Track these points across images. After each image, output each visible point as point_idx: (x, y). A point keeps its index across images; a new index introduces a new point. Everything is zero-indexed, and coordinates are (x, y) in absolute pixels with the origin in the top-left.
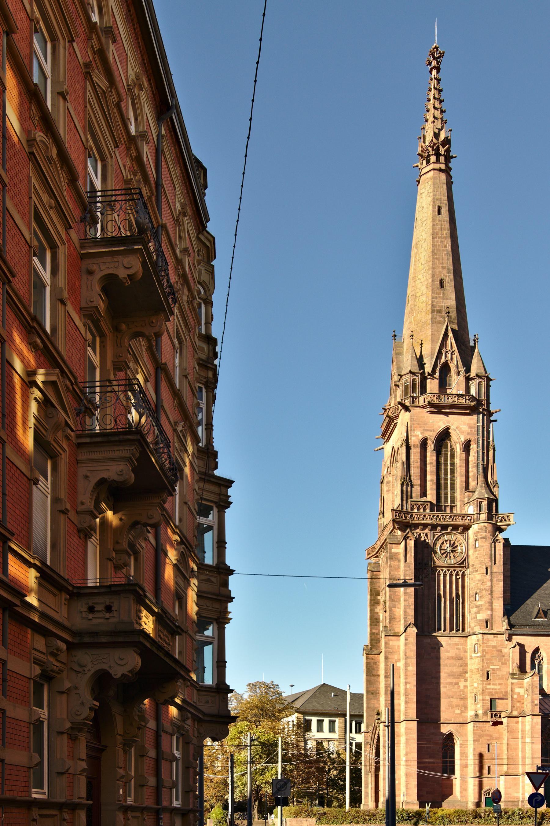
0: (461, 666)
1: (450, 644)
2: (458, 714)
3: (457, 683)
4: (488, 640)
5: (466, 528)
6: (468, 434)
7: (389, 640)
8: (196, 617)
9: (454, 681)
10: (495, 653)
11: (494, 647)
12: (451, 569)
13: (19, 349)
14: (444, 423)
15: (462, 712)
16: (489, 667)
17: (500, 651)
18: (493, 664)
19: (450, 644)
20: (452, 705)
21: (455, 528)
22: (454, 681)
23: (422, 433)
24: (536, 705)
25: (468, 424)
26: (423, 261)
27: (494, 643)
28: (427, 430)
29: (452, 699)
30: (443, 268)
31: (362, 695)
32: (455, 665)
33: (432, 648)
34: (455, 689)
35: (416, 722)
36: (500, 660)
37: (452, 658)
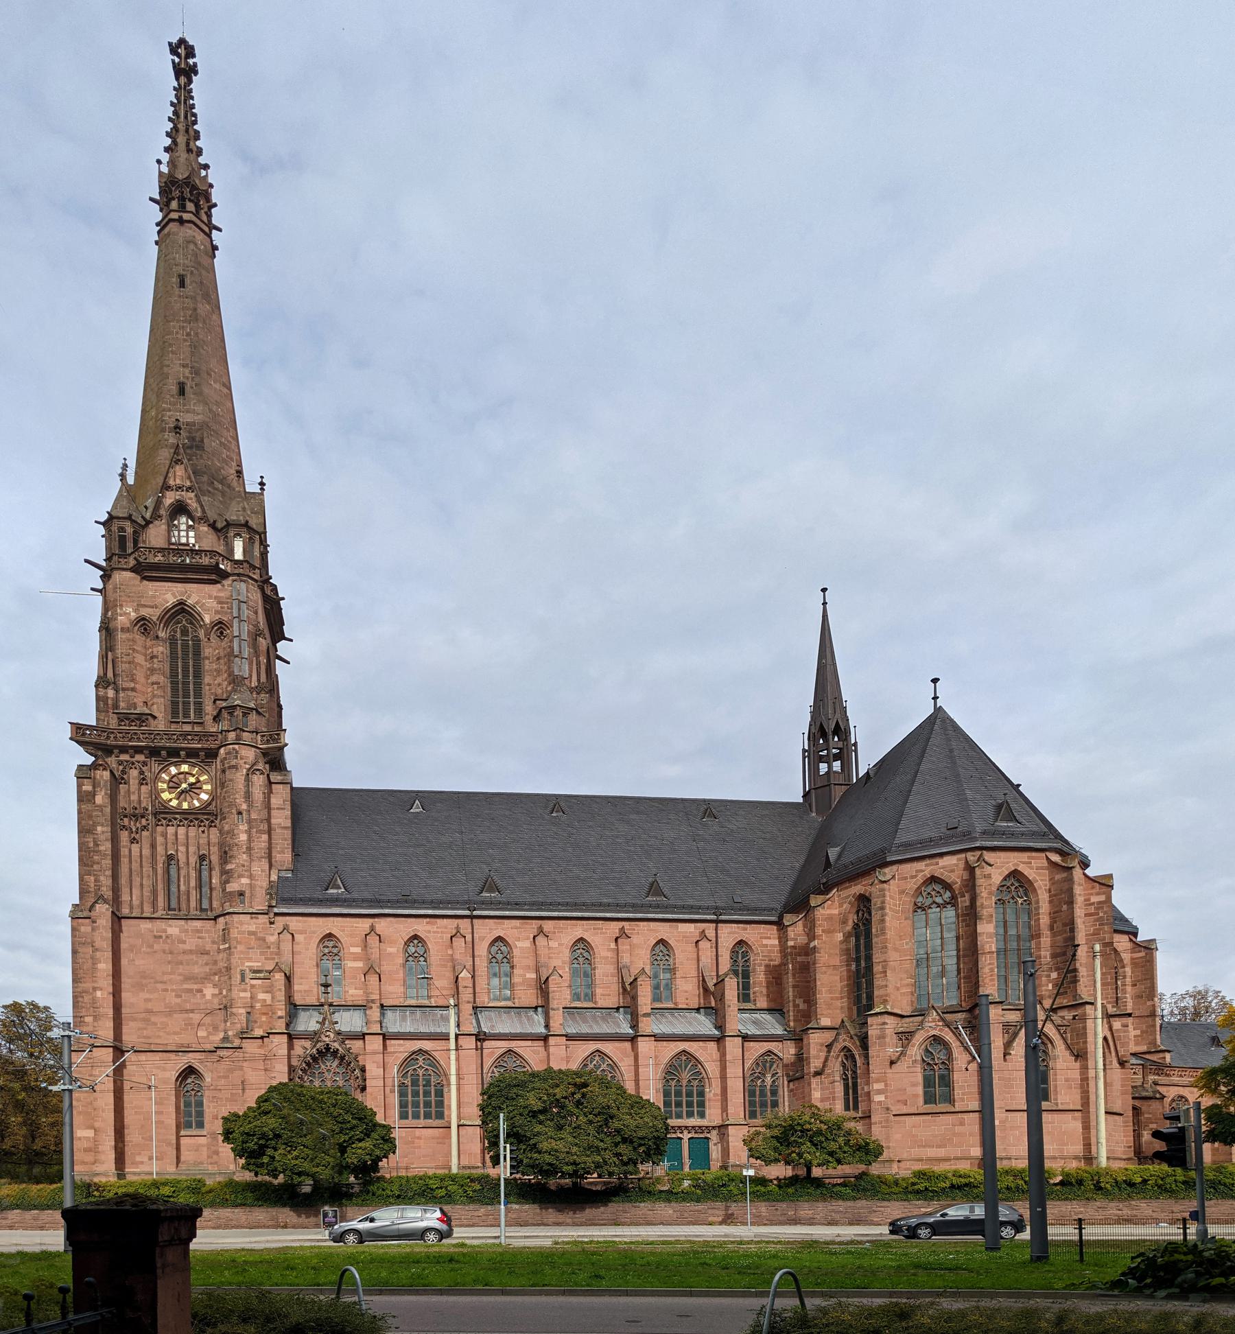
0: (207, 964)
3: (200, 991)
4: (241, 923)
6: (217, 612)
7: (79, 925)
9: (196, 987)
11: (253, 933)
13: (1093, 1132)
14: (174, 595)
16: (243, 964)
17: (264, 940)
18: (250, 960)
19: (187, 931)
22: (196, 987)
23: (136, 611)
24: (280, 1017)
25: (216, 598)
27: (253, 928)
29: (191, 1015)
31: (702, 1115)
32: (196, 963)
33: (155, 937)
34: (197, 998)
35: (111, 1050)
37: (191, 952)
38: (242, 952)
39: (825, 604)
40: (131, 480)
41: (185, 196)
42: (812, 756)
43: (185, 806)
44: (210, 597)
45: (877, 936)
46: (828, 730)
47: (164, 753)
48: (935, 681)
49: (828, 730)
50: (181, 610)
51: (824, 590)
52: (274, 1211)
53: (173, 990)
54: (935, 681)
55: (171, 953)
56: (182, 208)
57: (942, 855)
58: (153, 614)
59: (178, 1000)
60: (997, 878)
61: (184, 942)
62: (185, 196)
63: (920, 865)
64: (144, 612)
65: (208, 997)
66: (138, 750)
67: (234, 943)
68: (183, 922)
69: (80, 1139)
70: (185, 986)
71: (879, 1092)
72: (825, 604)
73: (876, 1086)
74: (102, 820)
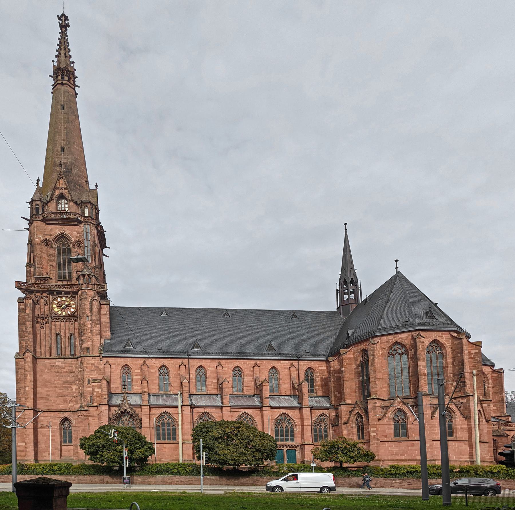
0: (73, 377)
1: (65, 363)
2: (71, 406)
3: (70, 387)
4: (88, 360)
5: (76, 293)
6: (77, 237)
8: (299, 405)
9: (68, 386)
10: (93, 368)
12: (67, 318)
14: (59, 230)
15: (74, 405)
16: (89, 377)
18: (92, 375)
20: (66, 401)
21: (67, 293)
22: (68, 386)
26: (423, 381)
27: (93, 362)
28: (47, 235)
30: (64, 140)
32: (69, 376)
36: (97, 373)
37: (66, 372)
38: (88, 372)
39: (346, 230)
40: (41, 185)
41: (64, 74)
42: (341, 292)
43: (64, 314)
44: (74, 231)
45: (371, 366)
46: (348, 281)
47: (55, 293)
48: (396, 261)
49: (348, 281)
50: (62, 236)
51: (346, 224)
52: (102, 477)
53: (59, 387)
54: (396, 261)
55: (58, 372)
56: (63, 79)
57: (400, 333)
58: (51, 238)
59: (61, 391)
60: (427, 343)
61: (64, 368)
62: (64, 74)
63: (391, 337)
64: (47, 237)
65: (74, 390)
66: (44, 292)
67: (85, 368)
68: (63, 360)
69: (19, 446)
70: (64, 386)
71: (374, 432)
72: (346, 230)
73: (372, 429)
74: (29, 319)
